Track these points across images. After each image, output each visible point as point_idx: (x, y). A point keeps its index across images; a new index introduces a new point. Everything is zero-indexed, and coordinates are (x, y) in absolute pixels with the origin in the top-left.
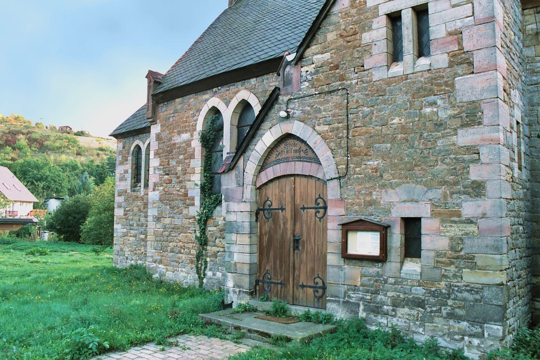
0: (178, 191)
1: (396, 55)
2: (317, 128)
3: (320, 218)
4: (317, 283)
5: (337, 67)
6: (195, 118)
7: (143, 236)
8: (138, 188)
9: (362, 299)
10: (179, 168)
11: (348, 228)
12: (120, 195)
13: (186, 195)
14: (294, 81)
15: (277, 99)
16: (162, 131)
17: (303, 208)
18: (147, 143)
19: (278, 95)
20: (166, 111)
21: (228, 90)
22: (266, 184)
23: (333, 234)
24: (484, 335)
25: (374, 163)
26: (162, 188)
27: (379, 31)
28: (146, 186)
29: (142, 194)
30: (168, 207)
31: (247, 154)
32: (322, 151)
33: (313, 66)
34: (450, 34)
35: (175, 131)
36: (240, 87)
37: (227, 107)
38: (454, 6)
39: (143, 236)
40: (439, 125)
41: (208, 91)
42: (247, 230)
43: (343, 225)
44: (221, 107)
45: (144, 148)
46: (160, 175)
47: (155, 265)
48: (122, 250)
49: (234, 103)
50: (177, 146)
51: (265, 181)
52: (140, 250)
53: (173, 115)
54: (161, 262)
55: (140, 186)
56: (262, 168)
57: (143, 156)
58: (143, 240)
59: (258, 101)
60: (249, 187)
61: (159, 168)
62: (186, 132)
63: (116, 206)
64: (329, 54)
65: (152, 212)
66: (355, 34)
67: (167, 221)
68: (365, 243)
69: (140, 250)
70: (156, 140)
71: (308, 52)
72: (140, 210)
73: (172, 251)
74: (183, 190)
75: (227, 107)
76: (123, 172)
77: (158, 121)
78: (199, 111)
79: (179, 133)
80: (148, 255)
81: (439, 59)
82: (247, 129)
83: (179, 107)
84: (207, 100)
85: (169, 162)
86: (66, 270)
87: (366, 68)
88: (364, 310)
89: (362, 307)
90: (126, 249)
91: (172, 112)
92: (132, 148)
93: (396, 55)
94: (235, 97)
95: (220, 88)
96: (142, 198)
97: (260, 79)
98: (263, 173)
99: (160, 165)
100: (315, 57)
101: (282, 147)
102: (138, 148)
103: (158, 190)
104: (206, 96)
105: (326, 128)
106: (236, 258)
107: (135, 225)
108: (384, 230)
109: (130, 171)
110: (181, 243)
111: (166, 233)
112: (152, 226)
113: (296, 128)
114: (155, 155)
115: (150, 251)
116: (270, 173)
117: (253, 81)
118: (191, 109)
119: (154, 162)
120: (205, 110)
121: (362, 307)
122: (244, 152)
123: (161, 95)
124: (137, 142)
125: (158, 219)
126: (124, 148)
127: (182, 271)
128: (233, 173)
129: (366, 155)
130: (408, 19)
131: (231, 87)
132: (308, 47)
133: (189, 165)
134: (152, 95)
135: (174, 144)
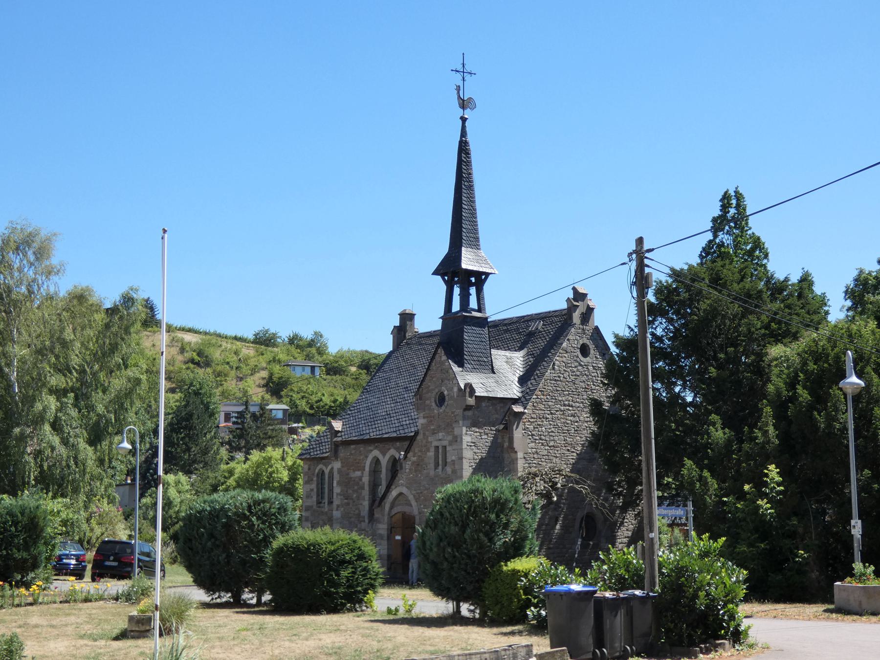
1: (437, 465)
13: (359, 514)
16: (342, 467)
18: (330, 467)
24: (406, 568)
27: (431, 454)
28: (331, 502)
32: (414, 503)
44: (380, 457)
45: (327, 471)
49: (388, 456)
56: (391, 508)
57: (326, 486)
62: (359, 470)
71: (409, 455)
78: (367, 457)
79: (354, 471)
83: (353, 452)
96: (326, 513)
101: (400, 498)
109: (315, 490)
113: (404, 490)
116: (396, 510)
117: (398, 444)
119: (337, 490)
124: (320, 466)
126: (309, 469)
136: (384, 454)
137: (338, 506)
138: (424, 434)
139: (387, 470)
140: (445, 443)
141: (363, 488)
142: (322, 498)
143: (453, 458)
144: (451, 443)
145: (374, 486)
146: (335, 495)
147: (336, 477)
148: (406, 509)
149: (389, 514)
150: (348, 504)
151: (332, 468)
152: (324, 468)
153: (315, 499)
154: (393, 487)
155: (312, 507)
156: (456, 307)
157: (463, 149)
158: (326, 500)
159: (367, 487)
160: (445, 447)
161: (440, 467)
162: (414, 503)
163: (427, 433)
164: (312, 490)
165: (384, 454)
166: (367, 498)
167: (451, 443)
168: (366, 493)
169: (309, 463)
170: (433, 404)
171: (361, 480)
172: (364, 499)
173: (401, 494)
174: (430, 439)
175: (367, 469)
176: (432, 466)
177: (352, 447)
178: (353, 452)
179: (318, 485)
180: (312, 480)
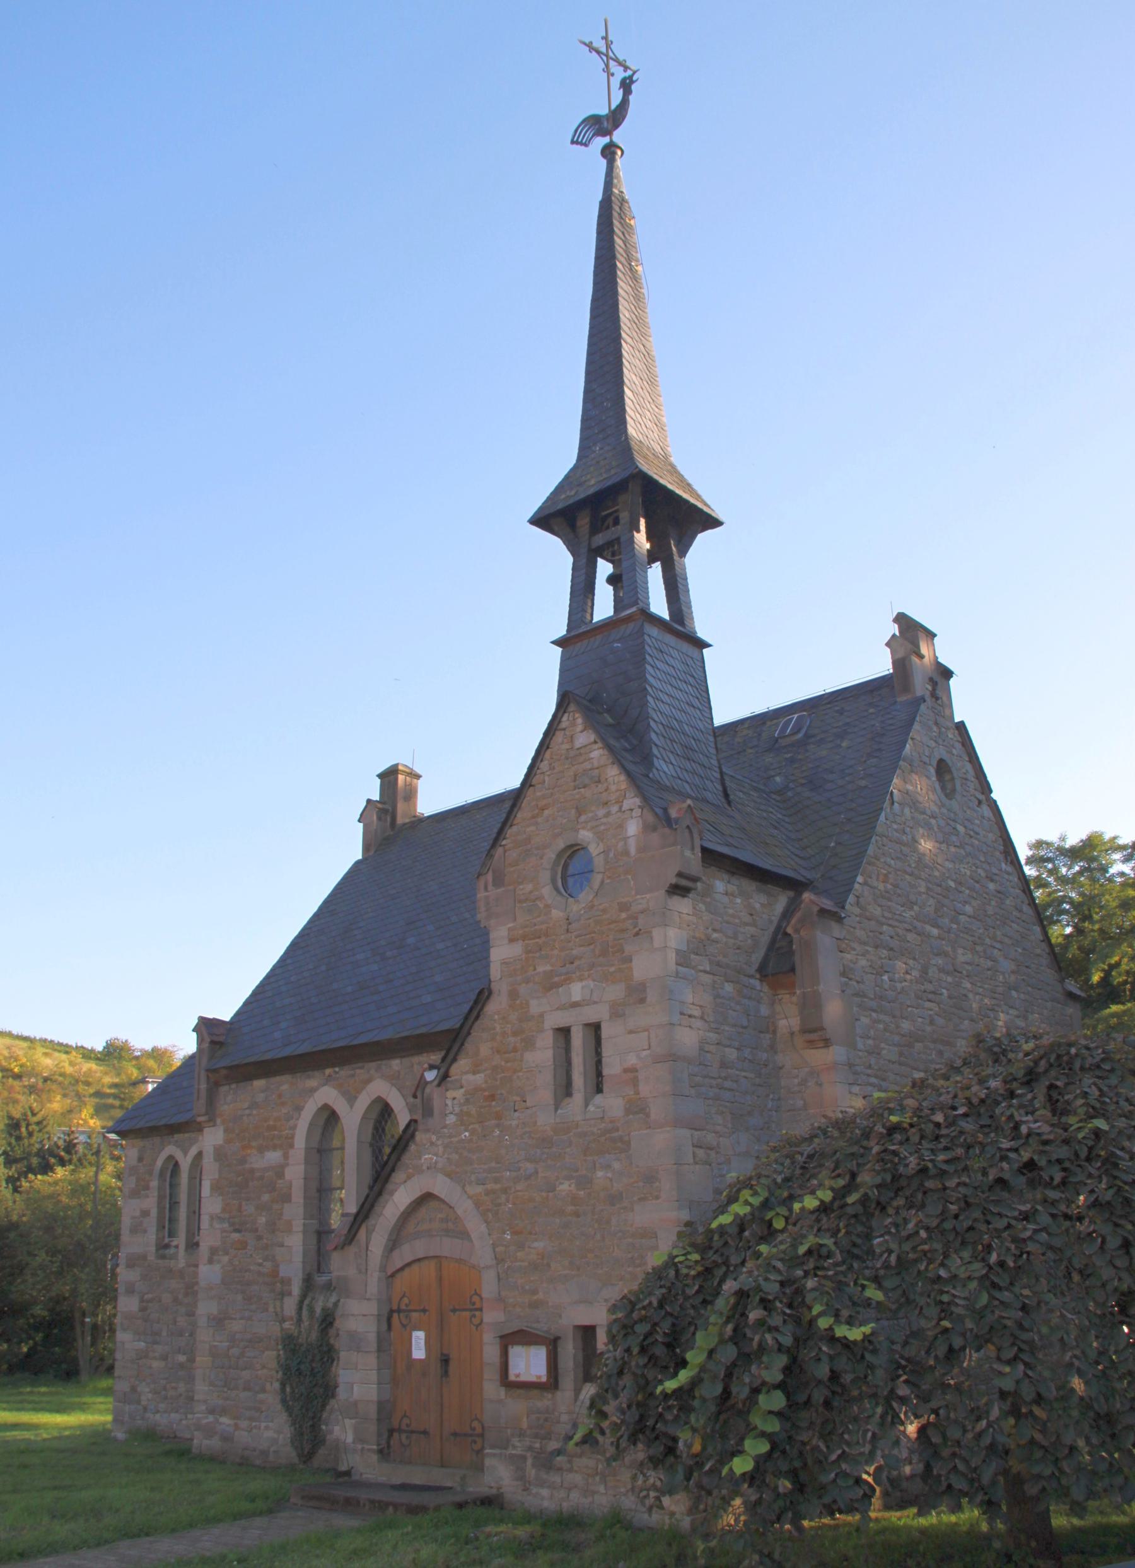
0: (260, 1265)
1: (565, 1089)
2: (468, 1188)
3: (477, 1326)
4: (474, 1429)
5: (492, 1097)
6: (292, 1122)
7: (182, 1358)
8: (172, 1251)
9: (530, 1448)
10: (262, 1220)
11: (509, 1339)
12: (130, 1265)
13: (275, 1273)
14: (436, 1112)
15: (413, 1136)
16: (228, 1141)
17: (454, 1310)
18: (193, 1151)
19: (415, 1130)
20: (233, 1101)
21: (353, 1076)
22: (402, 1269)
23: (491, 1352)
25: (539, 1245)
26: (226, 1259)
27: (543, 1054)
28: (192, 1245)
29: (182, 1263)
30: (239, 1297)
31: (371, 1221)
32: (475, 1225)
33: (462, 1090)
34: (626, 1071)
35: (254, 1144)
36: (372, 1072)
37: (351, 1107)
38: (631, 1032)
39: (182, 1358)
40: (614, 1199)
41: (316, 1074)
42: (373, 1346)
43: (502, 1337)
45: (185, 1163)
46: (223, 1231)
47: (211, 1418)
48: (134, 1389)
49: (363, 1101)
50: (258, 1174)
51: (399, 1265)
52: (175, 1388)
53: (247, 1112)
54: (224, 1411)
55: (177, 1247)
56: (394, 1243)
57: (182, 1213)
58: (181, 1366)
59: (404, 1104)
60: (376, 1275)
61: (219, 1218)
62: (275, 1148)
63: (121, 1289)
64: (482, 1075)
65: (206, 1308)
66: (515, 1050)
67: (236, 1326)
68: (530, 1364)
69: (175, 1388)
70: (216, 1160)
71: (455, 1070)
72: (176, 1300)
73: (247, 1388)
74: (268, 1264)
75: (351, 1107)
76: (138, 1213)
77: (219, 1121)
78: (299, 1109)
79: (261, 1150)
80: (196, 1398)
81: (612, 1103)
82: (387, 1150)
84: (313, 1090)
85: (240, 1206)
86: (66, 1428)
87: (528, 1104)
88: (533, 1465)
89: (529, 1462)
90: (144, 1389)
91: (246, 1105)
92: (159, 1163)
93: (565, 1089)
94: (364, 1092)
95: (337, 1069)
97: (406, 1061)
98: (396, 1253)
99: (224, 1210)
100: (464, 1077)
101: (423, 1212)
102: (174, 1167)
103: (219, 1262)
104: (312, 1083)
105: (480, 1189)
106: (358, 1392)
107: (164, 1333)
108: (553, 1345)
109: (154, 1212)
110: (265, 1371)
111: (235, 1351)
112: (205, 1336)
113: (441, 1186)
114: (212, 1189)
115: (201, 1388)
116: (405, 1253)
117: (396, 1064)
118: (283, 1104)
119: (211, 1205)
120: (310, 1108)
121: (529, 1462)
122: (367, 1217)
123: (224, 1072)
124: (171, 1150)
125: (219, 1322)
126: (140, 1159)
127: (267, 1428)
128: (352, 1250)
129: (530, 1233)
130: (578, 1039)
131: (358, 1071)
132: (454, 1060)
133: (281, 1214)
134: (207, 1070)
135: (252, 1171)
136: (351, 1100)
137: (213, 1251)
138: (513, 994)
139: (359, 1142)
140: (591, 1014)
141: (287, 1198)
142: (172, 1234)
143: (632, 1060)
144: (617, 1013)
145: (320, 1192)
146: (205, 1219)
147: (210, 1166)
148: (447, 1247)
149: (383, 1268)
150: (243, 1245)
151: (200, 1155)
152: (179, 1155)
153: (152, 1236)
154: (398, 1176)
155: (144, 1257)
156: (604, 605)
157: (610, 214)
158: (181, 1240)
159: (298, 1195)
160: (595, 1029)
161: (578, 1097)
162: (475, 1225)
163: (523, 989)
164: (145, 1213)
165: (351, 1100)
166: (298, 1225)
167: (617, 1013)
168: (295, 1211)
169: (139, 1143)
170: (547, 891)
171: (280, 1174)
172: (289, 1230)
173: (427, 1198)
174: (535, 1007)
175: (300, 1141)
176: (545, 1094)
177: (259, 1083)
178: (260, 1097)
179: (161, 1198)
180: (147, 1188)
